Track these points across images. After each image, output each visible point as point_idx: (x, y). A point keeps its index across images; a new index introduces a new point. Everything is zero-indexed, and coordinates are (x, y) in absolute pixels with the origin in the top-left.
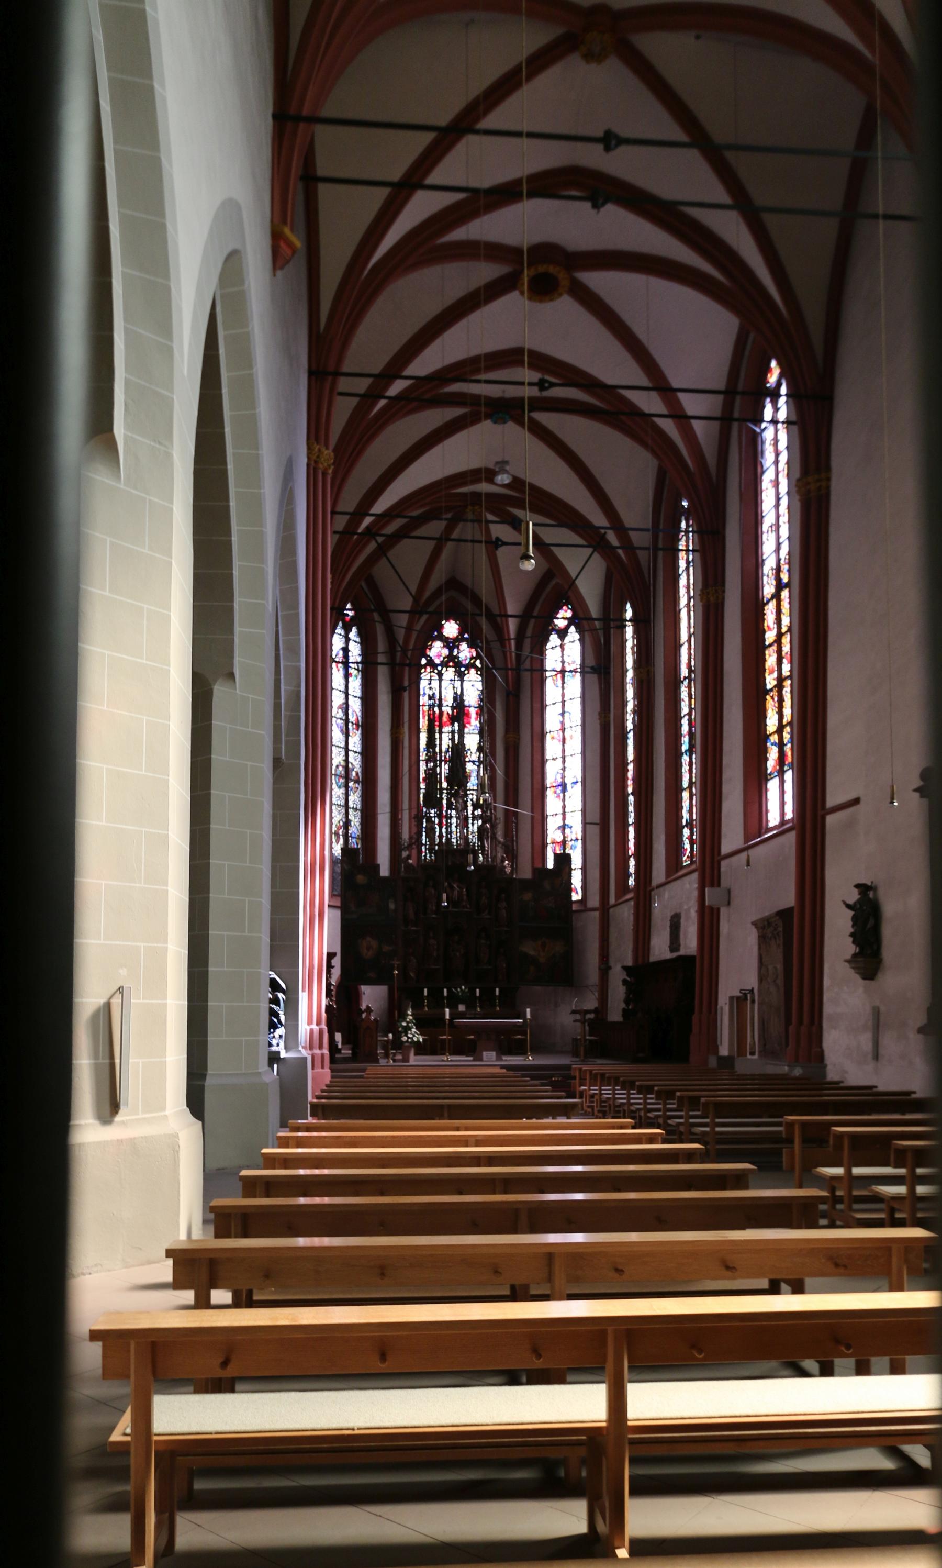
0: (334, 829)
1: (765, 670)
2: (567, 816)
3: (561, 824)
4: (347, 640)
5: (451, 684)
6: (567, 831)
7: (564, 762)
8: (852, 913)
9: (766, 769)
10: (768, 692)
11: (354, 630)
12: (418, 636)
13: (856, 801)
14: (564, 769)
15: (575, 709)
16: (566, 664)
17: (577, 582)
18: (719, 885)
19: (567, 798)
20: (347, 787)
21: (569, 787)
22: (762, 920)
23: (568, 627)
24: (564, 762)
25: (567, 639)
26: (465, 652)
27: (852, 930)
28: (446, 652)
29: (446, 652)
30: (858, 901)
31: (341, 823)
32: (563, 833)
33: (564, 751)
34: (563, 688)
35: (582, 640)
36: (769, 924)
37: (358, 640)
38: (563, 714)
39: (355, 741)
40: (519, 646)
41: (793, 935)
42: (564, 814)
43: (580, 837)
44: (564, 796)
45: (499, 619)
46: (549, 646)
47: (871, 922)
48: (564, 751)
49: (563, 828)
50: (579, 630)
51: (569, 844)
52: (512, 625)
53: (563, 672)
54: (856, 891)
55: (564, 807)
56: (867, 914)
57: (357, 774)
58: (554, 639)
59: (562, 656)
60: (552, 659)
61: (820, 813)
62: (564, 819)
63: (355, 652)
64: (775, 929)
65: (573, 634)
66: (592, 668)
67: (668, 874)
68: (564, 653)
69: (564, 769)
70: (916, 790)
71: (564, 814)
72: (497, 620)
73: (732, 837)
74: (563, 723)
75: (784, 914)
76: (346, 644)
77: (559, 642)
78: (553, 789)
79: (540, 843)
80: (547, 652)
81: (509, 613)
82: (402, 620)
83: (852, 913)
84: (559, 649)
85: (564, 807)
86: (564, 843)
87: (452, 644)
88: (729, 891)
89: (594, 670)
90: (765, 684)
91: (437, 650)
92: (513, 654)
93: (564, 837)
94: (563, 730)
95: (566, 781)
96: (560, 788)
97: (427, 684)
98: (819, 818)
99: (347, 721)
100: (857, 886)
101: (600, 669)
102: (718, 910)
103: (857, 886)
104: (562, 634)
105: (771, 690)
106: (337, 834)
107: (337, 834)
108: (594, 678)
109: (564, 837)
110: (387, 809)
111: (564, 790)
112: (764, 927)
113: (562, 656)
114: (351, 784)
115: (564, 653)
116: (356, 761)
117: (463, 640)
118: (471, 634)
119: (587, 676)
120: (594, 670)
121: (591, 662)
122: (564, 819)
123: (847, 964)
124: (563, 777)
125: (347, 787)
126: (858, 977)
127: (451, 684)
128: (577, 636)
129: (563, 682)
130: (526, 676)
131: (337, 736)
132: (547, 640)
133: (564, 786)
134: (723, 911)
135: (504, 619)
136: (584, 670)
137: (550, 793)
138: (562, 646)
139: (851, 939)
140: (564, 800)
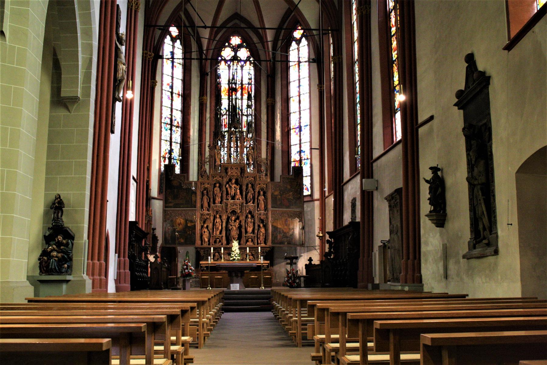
0: (162, 154)
1: (392, 49)
2: (302, 145)
3: (298, 150)
4: (174, 47)
5: (236, 70)
6: (302, 154)
7: (300, 114)
8: (429, 185)
9: (395, 107)
10: (393, 62)
11: (178, 41)
12: (217, 44)
13: (432, 118)
14: (300, 118)
15: (305, 83)
16: (300, 59)
17: (299, 6)
18: (372, 177)
19: (302, 135)
20: (171, 130)
21: (303, 128)
22: (389, 196)
23: (301, 38)
24: (300, 114)
25: (301, 45)
26: (243, 53)
27: (429, 196)
28: (233, 54)
29: (233, 54)
30: (432, 178)
31: (167, 151)
32: (300, 155)
33: (300, 108)
34: (299, 72)
35: (308, 45)
36: (393, 198)
37: (181, 47)
38: (299, 86)
39: (178, 103)
40: (274, 48)
41: (403, 202)
42: (300, 144)
43: (309, 157)
44: (300, 134)
45: (260, 31)
46: (291, 49)
47: (440, 190)
48: (300, 108)
49: (300, 152)
50: (307, 39)
51: (303, 162)
52: (270, 36)
53: (299, 62)
54: (430, 171)
55: (300, 140)
56: (438, 185)
57: (178, 123)
58: (294, 45)
59: (299, 54)
60: (293, 56)
61: (415, 127)
62: (300, 147)
63: (179, 53)
64: (396, 200)
65: (304, 42)
66: (313, 59)
67: (351, 173)
68: (300, 52)
69: (300, 118)
70: (455, 105)
71: (300, 144)
72: (260, 32)
73: (378, 149)
74: (299, 92)
75: (398, 191)
76: (172, 48)
77: (296, 46)
78: (294, 130)
79: (287, 161)
80: (290, 52)
81: (266, 27)
82: (206, 34)
83: (429, 185)
84: (296, 50)
85: (300, 140)
86: (300, 161)
87: (236, 49)
88: (377, 181)
89: (314, 61)
90: (392, 58)
91: (227, 53)
92: (271, 53)
93: (301, 158)
94: (299, 96)
95: (302, 125)
96: (298, 129)
97: (223, 70)
98: (415, 130)
99: (172, 93)
100: (431, 168)
101: (317, 60)
102: (372, 192)
103: (431, 168)
104: (298, 42)
105: (395, 60)
106: (165, 158)
107: (165, 158)
108: (315, 65)
109: (301, 158)
110: (196, 142)
111: (300, 131)
112: (390, 198)
113: (299, 54)
114: (174, 128)
115: (300, 52)
116: (178, 117)
117: (243, 47)
118: (247, 43)
119: (311, 64)
120: (314, 61)
121: (313, 57)
122: (300, 147)
123: (427, 217)
124: (300, 123)
125: (171, 130)
126: (433, 225)
127: (236, 70)
128: (306, 43)
129: (299, 69)
130: (279, 65)
131: (167, 102)
132: (290, 45)
133: (300, 128)
134: (375, 193)
135: (263, 30)
136: (310, 61)
137: (292, 132)
138: (298, 49)
139: (429, 201)
140: (300, 136)
